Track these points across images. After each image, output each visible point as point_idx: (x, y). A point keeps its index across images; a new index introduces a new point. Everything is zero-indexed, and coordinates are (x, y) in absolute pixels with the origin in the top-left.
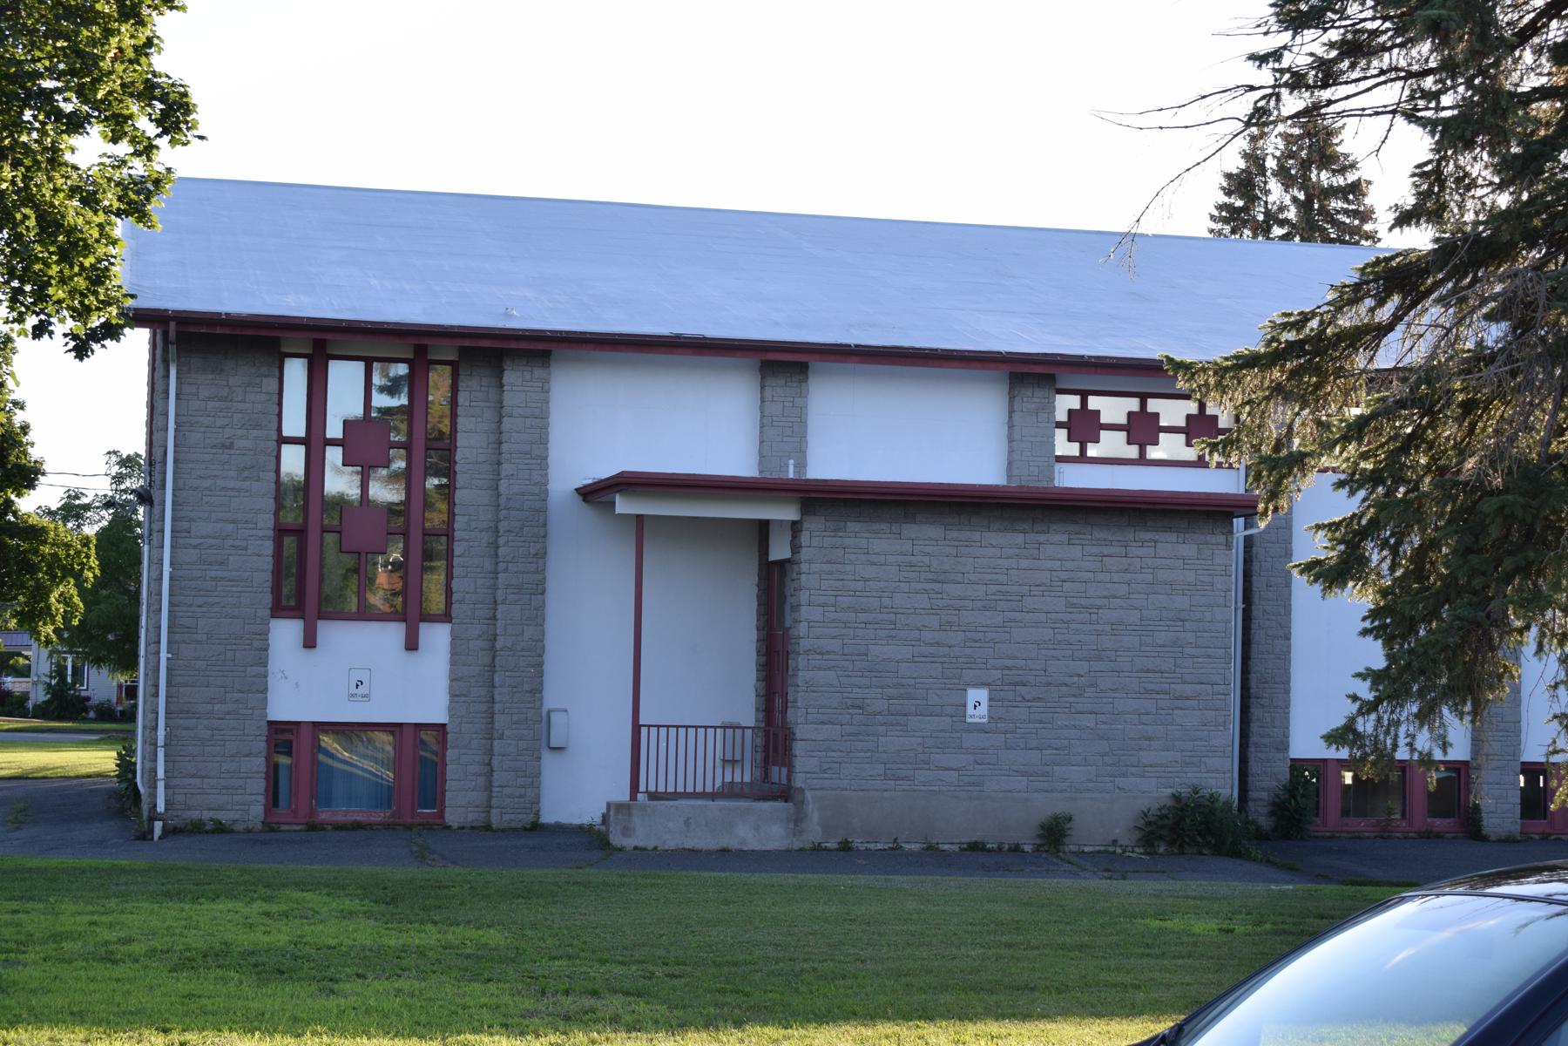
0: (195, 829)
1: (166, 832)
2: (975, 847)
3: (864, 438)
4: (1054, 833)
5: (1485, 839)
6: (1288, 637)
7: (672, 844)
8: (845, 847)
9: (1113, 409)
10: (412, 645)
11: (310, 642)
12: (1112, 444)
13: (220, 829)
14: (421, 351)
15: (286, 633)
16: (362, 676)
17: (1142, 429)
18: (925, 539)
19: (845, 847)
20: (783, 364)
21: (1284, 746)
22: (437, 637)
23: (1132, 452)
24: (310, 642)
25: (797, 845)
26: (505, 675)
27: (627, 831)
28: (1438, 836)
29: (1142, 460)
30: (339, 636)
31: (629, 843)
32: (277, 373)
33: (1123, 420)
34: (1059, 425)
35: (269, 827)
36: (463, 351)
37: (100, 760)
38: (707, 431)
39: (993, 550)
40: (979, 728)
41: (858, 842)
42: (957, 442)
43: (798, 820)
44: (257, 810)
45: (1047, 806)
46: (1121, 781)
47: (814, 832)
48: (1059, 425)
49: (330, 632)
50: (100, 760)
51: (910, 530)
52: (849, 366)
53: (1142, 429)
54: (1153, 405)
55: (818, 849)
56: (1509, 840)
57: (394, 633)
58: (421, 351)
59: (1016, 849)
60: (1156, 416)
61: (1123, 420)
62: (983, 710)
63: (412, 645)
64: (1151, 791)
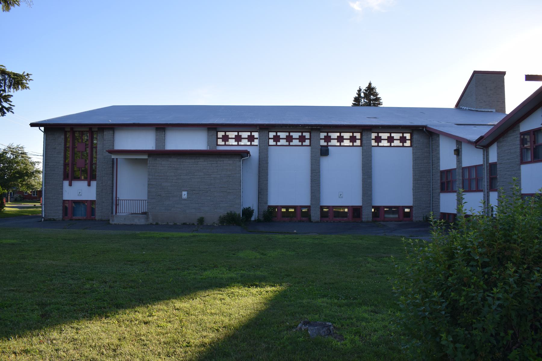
0: (50, 220)
1: (44, 220)
2: (184, 224)
3: (177, 142)
4: (201, 221)
5: (312, 222)
6: (267, 180)
7: (122, 223)
8: (157, 224)
9: (283, 135)
10: (89, 185)
11: (70, 185)
12: (232, 142)
13: (54, 220)
14: (90, 129)
15: (66, 183)
16: (80, 191)
17: (238, 138)
18: (188, 163)
19: (157, 224)
20: (161, 128)
21: (267, 203)
22: (94, 183)
23: (401, 144)
24: (70, 185)
25: (147, 223)
26: (109, 190)
27: (113, 221)
28: (303, 221)
29: (238, 145)
30: (76, 183)
31: (113, 223)
32: (107, 135)
33: (298, 137)
34: (373, 139)
35: (63, 220)
36: (98, 128)
37: (397, 216)
38: (146, 142)
39: (202, 163)
40: (185, 200)
41: (160, 223)
42: (197, 142)
43: (147, 218)
44: (61, 217)
45: (199, 215)
46: (216, 210)
47: (151, 221)
48: (373, 139)
49: (75, 183)
50: (397, 216)
51: (170, 160)
52: (175, 128)
53: (238, 138)
54: (227, 133)
55: (151, 224)
56: (317, 222)
57: (86, 183)
58: (90, 129)
59: (193, 224)
60: (381, 137)
61: (298, 137)
62: (186, 196)
63: (89, 185)
64: (223, 212)
